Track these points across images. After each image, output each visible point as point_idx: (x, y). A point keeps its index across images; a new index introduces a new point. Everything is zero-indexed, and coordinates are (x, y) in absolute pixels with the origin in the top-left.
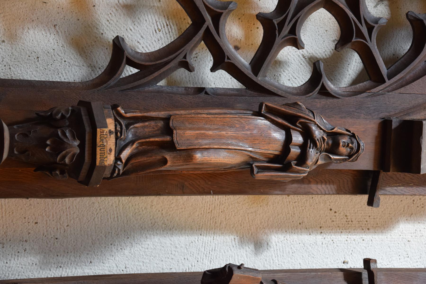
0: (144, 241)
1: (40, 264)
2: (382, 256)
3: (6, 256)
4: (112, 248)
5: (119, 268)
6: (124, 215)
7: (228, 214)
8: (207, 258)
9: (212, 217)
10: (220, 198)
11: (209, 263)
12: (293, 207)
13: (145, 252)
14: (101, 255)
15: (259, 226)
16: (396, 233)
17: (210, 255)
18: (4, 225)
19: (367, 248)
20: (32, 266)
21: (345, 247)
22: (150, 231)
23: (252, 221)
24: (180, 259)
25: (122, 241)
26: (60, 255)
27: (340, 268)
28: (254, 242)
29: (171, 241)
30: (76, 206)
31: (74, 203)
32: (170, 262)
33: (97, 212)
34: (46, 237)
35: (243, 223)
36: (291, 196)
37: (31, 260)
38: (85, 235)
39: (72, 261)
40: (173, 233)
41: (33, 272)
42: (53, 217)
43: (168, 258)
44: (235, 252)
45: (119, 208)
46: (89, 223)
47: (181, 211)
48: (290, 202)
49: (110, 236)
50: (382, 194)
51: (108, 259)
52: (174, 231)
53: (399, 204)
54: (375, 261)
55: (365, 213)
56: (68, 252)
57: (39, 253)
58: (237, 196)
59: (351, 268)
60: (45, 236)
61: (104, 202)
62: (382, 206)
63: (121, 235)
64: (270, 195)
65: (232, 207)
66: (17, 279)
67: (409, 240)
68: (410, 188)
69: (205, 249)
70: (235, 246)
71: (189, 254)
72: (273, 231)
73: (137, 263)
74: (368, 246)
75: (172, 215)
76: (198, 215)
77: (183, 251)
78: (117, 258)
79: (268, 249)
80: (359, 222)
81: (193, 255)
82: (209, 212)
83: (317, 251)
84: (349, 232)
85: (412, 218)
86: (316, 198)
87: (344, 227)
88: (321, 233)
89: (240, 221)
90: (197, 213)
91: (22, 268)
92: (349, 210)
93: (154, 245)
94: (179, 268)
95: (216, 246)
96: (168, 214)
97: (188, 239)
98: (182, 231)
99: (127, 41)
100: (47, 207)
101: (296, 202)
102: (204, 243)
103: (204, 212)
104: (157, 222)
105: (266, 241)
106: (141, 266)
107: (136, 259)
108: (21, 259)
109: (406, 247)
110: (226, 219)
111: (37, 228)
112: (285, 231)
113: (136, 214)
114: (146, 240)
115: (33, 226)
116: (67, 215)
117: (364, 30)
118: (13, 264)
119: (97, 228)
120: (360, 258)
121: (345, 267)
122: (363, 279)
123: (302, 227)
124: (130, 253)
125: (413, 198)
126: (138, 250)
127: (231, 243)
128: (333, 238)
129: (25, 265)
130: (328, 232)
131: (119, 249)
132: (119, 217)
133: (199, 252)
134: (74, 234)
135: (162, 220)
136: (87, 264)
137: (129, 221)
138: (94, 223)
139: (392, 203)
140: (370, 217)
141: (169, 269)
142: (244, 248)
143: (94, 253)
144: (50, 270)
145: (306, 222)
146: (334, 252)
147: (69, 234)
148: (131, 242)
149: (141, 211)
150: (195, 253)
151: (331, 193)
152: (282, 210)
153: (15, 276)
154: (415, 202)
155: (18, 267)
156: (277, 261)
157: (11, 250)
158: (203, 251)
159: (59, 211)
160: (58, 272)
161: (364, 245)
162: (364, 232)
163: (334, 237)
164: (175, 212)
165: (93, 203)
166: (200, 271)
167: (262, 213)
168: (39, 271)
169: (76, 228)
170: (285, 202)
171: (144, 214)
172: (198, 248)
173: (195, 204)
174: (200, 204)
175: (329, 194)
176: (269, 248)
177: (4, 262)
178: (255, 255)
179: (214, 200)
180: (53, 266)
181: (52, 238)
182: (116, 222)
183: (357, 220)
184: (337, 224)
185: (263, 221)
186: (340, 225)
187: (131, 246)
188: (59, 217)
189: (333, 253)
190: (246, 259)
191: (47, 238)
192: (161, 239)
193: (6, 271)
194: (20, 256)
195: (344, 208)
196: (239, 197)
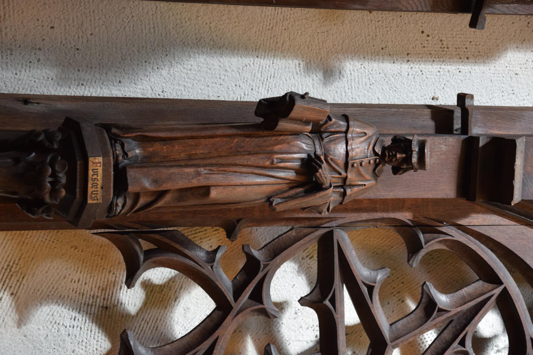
0: (187, 60)
1: (57, 78)
2: (481, 92)
3: (15, 65)
4: (146, 66)
5: (154, 91)
6: (162, 26)
7: (293, 33)
8: (264, 86)
9: (272, 36)
10: (284, 12)
11: (266, 92)
12: (376, 27)
13: (187, 74)
14: (132, 74)
15: (331, 49)
16: (501, 64)
17: (268, 83)
18: (11, 27)
19: (464, 81)
20: (47, 80)
21: (436, 80)
22: (194, 48)
23: (323, 43)
24: (230, 85)
25: (159, 58)
26: (82, 70)
27: (428, 104)
28: (324, 69)
29: (220, 62)
30: (102, 10)
31: (100, 5)
32: (218, 88)
33: (129, 20)
34: (64, 47)
35: (311, 44)
36: (374, 13)
37: (46, 73)
38: (113, 47)
39: (96, 78)
40: (223, 53)
41: (48, 88)
42: (73, 22)
43: (216, 83)
44: (299, 80)
45: (156, 17)
46: (118, 33)
47: (234, 25)
48: (371, 21)
49: (144, 51)
50: (489, 12)
51: (141, 80)
52: (225, 51)
53: (509, 27)
54: (472, 97)
55: (465, 38)
56: (91, 68)
57: (56, 65)
58: (306, 9)
59: (441, 105)
60: (64, 45)
61: (137, 7)
62: (488, 29)
63: (158, 50)
64: (348, 9)
65: (298, 24)
66: (29, 94)
67: (517, 72)
68: (526, 5)
69: (261, 74)
70: (299, 73)
71: (242, 80)
72: (348, 57)
73: (177, 87)
74: (465, 80)
75: (223, 30)
76: (255, 32)
77: (234, 75)
78: (152, 80)
79: (340, 78)
80: (456, 49)
81: (247, 81)
82: (269, 29)
83: (400, 83)
84: (443, 61)
85: (524, 45)
86: (405, 16)
87: (437, 54)
88: (408, 61)
89: (308, 43)
90: (254, 29)
91: (35, 82)
92: (446, 34)
93: (199, 66)
94: (229, 96)
95: (276, 72)
96: (218, 29)
97: (242, 61)
98: (234, 50)
100: (66, 8)
101: (380, 21)
102: (261, 67)
103: (263, 29)
104: (203, 37)
105: (338, 69)
106: (181, 91)
107: (175, 82)
108: (34, 71)
109: (513, 81)
110: (289, 38)
111: (53, 34)
112: (362, 58)
113: (178, 26)
114: (189, 59)
115: (48, 31)
116: (91, 21)
118: (24, 77)
119: (128, 39)
120: (454, 94)
121: (434, 103)
122: (455, 119)
123: (385, 53)
124: (169, 74)
125: (528, 19)
126: (179, 70)
127: (294, 69)
128: (422, 67)
129: (39, 79)
130: (417, 60)
131: (155, 68)
132: (156, 29)
133: (254, 78)
134: (100, 45)
135: (210, 36)
136: (115, 84)
137: (168, 34)
138: (124, 33)
139: (501, 26)
140: (472, 43)
141: (216, 97)
142: (311, 76)
143: (124, 71)
144: (70, 88)
145: (390, 47)
146: (422, 85)
147: (93, 45)
148: (171, 61)
149: (184, 22)
150: (249, 78)
151: (425, 9)
152: (361, 31)
153: (26, 91)
154: (529, 25)
155: (31, 80)
156: (350, 94)
157: (21, 59)
158: (260, 77)
159: (81, 14)
160: (79, 90)
161: (461, 78)
162: (462, 61)
163: (424, 66)
164: (227, 26)
165: (124, 8)
166: (255, 101)
167: (336, 33)
168: (56, 88)
169: (103, 37)
170: (366, 20)
171: (187, 27)
172: (253, 74)
173: (252, 18)
174: (258, 18)
175: (422, 11)
176: (341, 77)
177: (12, 73)
178: (324, 85)
179: (276, 13)
180: (73, 82)
181: (72, 48)
182: (152, 34)
183: (454, 46)
184: (428, 51)
185: (336, 43)
186: (432, 52)
187: (170, 66)
188: (80, 22)
189: (421, 86)
190: (312, 89)
191: (66, 47)
192: (207, 59)
193: (16, 83)
194: (32, 66)
195: (439, 30)
196: (308, 12)
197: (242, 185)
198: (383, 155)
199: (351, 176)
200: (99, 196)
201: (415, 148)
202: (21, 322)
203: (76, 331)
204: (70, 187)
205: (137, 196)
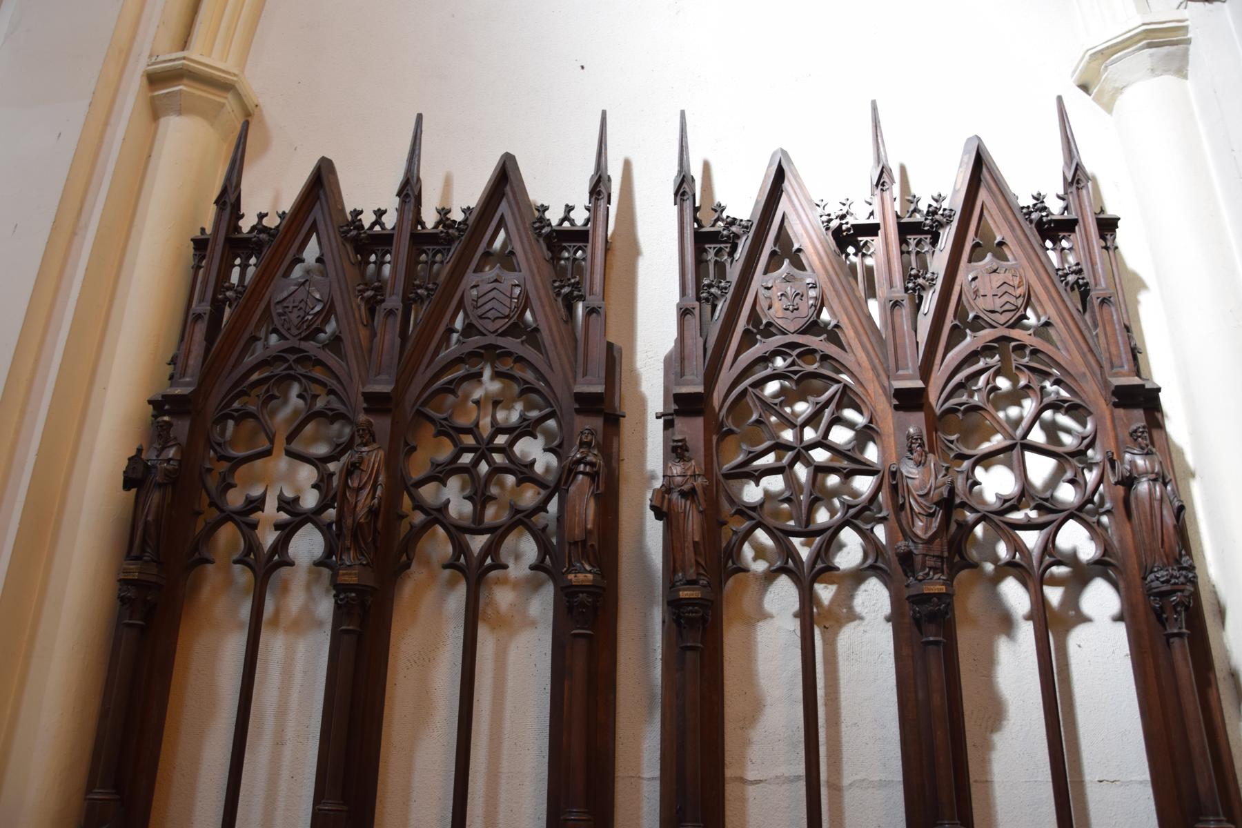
99: (530, 563)
117: (526, 423)
197: (693, 526)
198: (681, 458)
199: (689, 473)
200: (697, 592)
201: (675, 444)
202: (771, 617)
203: (776, 591)
204: (694, 605)
205: (699, 574)
